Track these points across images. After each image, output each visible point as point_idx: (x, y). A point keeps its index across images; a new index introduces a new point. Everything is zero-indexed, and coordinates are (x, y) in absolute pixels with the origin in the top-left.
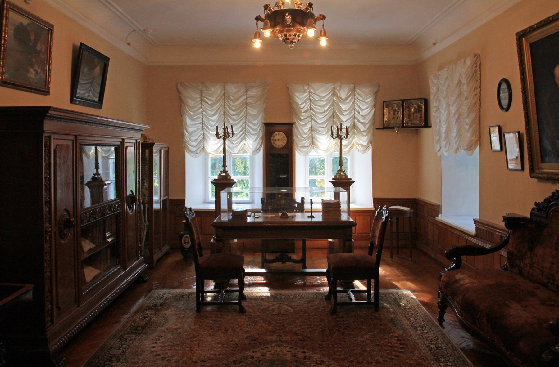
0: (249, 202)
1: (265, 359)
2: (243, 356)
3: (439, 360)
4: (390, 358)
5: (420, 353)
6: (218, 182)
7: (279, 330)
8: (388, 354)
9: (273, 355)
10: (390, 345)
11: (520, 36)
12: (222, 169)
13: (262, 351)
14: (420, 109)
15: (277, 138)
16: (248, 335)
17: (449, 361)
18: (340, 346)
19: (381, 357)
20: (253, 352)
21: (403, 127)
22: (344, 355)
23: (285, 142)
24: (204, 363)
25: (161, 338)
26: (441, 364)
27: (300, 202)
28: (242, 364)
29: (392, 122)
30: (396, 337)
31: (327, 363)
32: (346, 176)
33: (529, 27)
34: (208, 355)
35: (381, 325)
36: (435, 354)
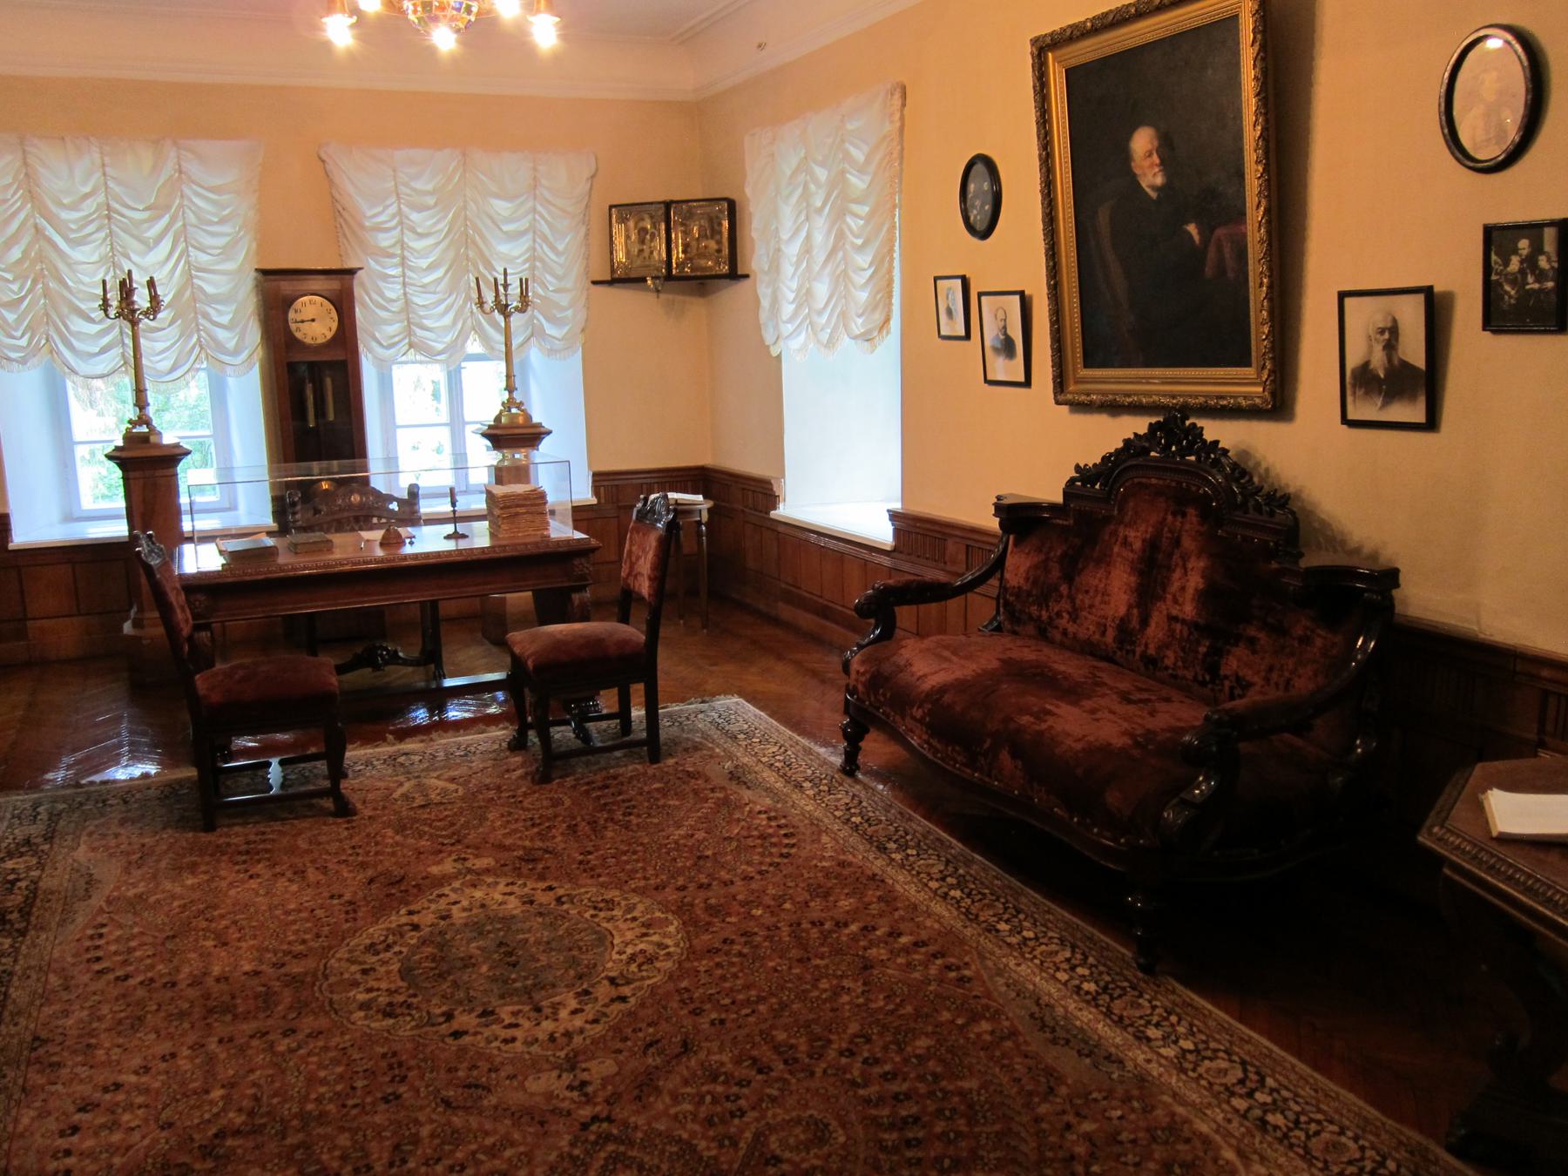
0: (217, 506)
1: (452, 924)
2: (388, 929)
3: (886, 848)
4: (771, 865)
5: (835, 839)
6: (124, 454)
7: (453, 844)
8: (762, 855)
9: (471, 910)
10: (755, 833)
11: (1043, 48)
12: (131, 413)
13: (433, 907)
14: (716, 227)
15: (308, 312)
16: (370, 873)
17: (907, 847)
18: (635, 857)
19: (749, 863)
20: (410, 913)
21: (669, 277)
22: (657, 876)
23: (335, 326)
24: (283, 970)
25: (104, 930)
26: (893, 856)
28: (397, 949)
29: (639, 262)
30: (760, 812)
31: (623, 903)
32: (528, 417)
33: (1070, 26)
34: (285, 947)
35: (713, 790)
36: (871, 837)
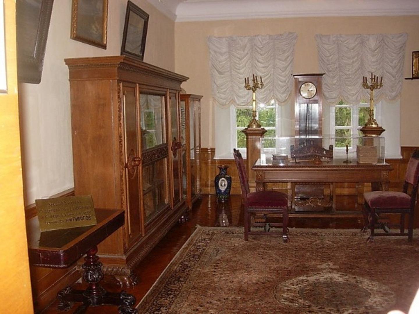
20: (307, 277)
27: (328, 149)
